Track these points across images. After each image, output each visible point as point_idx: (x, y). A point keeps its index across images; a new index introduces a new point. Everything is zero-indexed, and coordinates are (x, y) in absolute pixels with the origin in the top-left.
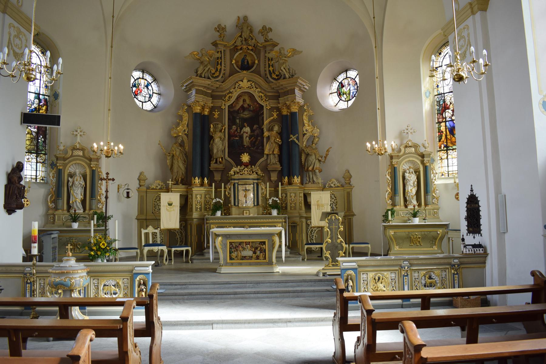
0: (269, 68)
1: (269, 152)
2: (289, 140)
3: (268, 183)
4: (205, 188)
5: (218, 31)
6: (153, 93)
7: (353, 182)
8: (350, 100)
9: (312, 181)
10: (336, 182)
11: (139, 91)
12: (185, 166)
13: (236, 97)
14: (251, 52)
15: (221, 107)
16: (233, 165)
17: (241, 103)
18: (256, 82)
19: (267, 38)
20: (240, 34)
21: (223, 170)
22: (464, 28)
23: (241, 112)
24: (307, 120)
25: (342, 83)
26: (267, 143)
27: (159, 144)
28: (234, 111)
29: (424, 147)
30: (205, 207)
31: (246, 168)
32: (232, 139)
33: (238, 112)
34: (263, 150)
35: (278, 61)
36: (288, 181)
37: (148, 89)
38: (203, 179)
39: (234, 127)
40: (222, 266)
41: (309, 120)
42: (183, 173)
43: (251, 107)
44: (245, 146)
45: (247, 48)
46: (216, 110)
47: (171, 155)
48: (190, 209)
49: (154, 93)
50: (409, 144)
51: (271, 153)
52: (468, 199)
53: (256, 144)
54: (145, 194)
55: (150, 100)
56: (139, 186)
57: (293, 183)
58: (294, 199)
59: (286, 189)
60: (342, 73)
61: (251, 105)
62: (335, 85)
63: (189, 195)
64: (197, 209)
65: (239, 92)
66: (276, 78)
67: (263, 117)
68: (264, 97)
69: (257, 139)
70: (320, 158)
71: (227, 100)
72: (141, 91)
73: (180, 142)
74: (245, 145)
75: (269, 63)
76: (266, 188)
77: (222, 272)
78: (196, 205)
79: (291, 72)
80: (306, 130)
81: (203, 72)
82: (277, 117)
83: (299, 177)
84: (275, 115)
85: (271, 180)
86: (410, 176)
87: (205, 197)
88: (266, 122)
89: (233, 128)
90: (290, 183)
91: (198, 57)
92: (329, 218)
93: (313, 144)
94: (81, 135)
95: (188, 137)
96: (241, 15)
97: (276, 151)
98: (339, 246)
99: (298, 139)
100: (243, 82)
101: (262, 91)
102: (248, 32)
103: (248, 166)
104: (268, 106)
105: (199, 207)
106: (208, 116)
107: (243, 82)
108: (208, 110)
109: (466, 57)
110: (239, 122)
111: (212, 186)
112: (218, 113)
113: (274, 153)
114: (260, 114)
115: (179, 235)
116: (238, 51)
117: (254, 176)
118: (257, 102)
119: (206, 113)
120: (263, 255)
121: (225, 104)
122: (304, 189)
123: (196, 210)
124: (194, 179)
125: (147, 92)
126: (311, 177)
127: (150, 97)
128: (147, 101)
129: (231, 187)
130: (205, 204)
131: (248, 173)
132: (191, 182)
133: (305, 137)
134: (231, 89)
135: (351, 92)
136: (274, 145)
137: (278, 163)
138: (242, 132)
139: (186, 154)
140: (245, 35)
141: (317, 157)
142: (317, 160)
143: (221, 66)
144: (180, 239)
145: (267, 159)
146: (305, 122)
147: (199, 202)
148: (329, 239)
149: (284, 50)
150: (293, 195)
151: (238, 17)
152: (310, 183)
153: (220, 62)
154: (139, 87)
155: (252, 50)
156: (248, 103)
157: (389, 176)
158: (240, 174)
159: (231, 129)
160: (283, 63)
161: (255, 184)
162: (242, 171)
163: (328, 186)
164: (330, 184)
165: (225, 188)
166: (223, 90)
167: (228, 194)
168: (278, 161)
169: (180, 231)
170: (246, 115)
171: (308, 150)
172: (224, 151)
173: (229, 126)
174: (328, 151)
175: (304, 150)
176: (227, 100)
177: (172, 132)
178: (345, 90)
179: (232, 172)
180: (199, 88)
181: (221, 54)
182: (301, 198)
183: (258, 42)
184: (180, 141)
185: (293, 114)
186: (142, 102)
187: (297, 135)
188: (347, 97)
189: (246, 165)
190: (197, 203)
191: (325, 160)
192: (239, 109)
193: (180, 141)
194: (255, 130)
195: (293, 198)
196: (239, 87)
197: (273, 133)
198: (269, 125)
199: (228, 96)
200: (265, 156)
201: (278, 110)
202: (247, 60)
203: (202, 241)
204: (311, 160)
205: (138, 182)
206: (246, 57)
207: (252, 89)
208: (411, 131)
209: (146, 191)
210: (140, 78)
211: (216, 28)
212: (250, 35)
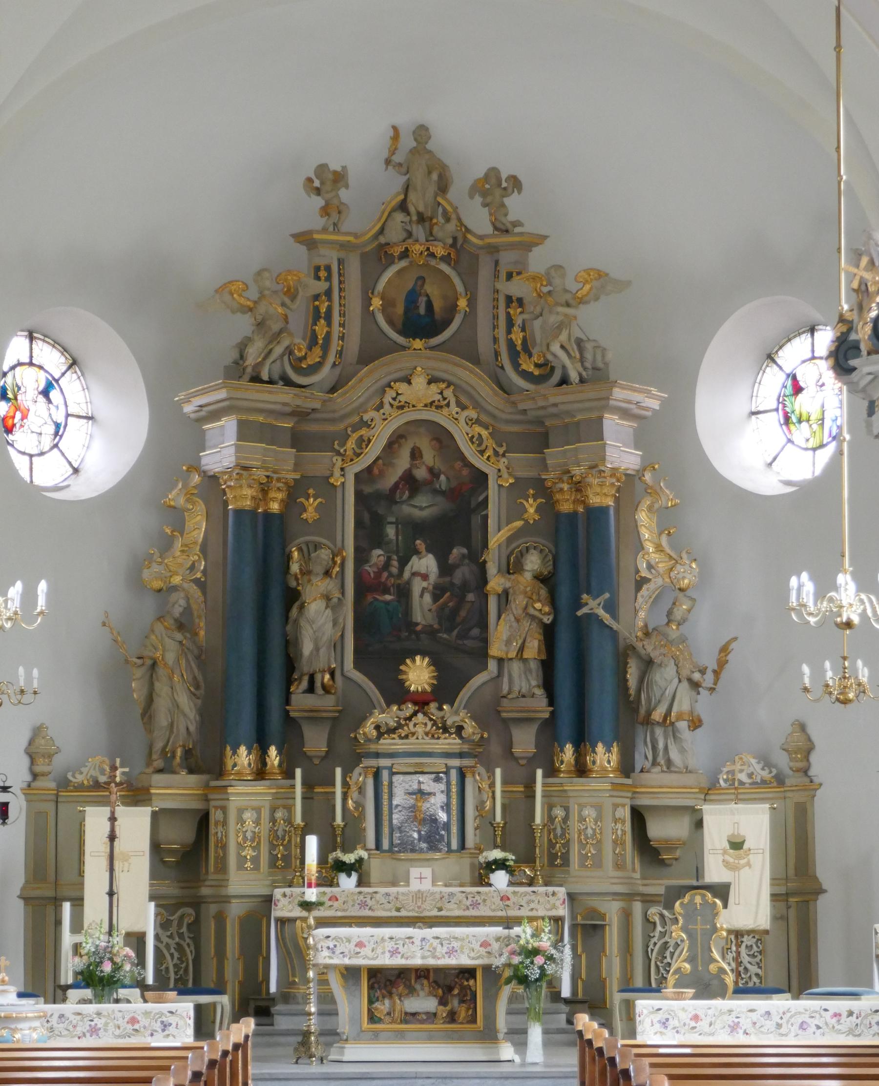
0: (509, 332)
1: (507, 654)
2: (579, 613)
3: (498, 772)
4: (270, 788)
5: (318, 192)
6: (68, 415)
7: (818, 766)
8: (822, 446)
9: (662, 762)
11: (18, 415)
12: (199, 702)
13: (384, 442)
14: (444, 267)
15: (328, 478)
16: (376, 703)
17: (403, 462)
18: (458, 382)
19: (503, 219)
20: (402, 197)
21: (334, 719)
23: (405, 497)
24: (654, 525)
26: (499, 617)
27: (104, 624)
28: (378, 496)
30: (239, 854)
31: (420, 716)
32: (370, 598)
33: (390, 498)
34: (485, 641)
35: (541, 315)
36: (577, 760)
37: (49, 401)
38: (264, 752)
39: (377, 555)
40: (347, 1040)
41: (662, 529)
42: (192, 728)
43: (443, 478)
44: (419, 628)
45: (428, 249)
46: (311, 491)
47: (149, 662)
48: (216, 863)
49: (73, 415)
51: (512, 654)
53: (459, 619)
54: (54, 808)
55: (56, 446)
56: (28, 778)
57: (591, 771)
58: (594, 830)
59: (565, 791)
60: (795, 337)
61: (443, 469)
63: (212, 811)
64: (242, 860)
65: (398, 421)
66: (537, 372)
67: (486, 518)
68: (491, 441)
69: (462, 599)
70: (697, 676)
71: (350, 453)
72: (25, 412)
73: (177, 615)
74: (417, 624)
75: (508, 314)
76: (492, 785)
77: (345, 1059)
78: (241, 847)
79: (589, 356)
80: (650, 567)
81: (265, 359)
82: (537, 517)
83: (615, 749)
84: (531, 510)
85: (512, 753)
87: (273, 820)
88: (496, 538)
89: (374, 560)
90: (581, 770)
91: (242, 301)
92: (686, 900)
93: (669, 622)
95: (204, 593)
96: (406, 120)
97: (534, 648)
98: (715, 982)
99: (611, 607)
100: (409, 383)
101: (484, 418)
102: (432, 189)
103: (427, 703)
104: (505, 475)
105: (249, 853)
106: (281, 516)
107: (409, 383)
108: (280, 496)
110: (397, 535)
111: (292, 776)
112: (319, 500)
113: (525, 656)
114: (473, 504)
115: (172, 955)
116: (393, 263)
117: (451, 743)
118: (463, 458)
119: (275, 507)
120: (468, 1009)
121: (342, 469)
122: (635, 793)
123: (241, 867)
124: (235, 753)
125: (45, 415)
126: (661, 745)
127: (56, 434)
128: (46, 448)
129: (364, 782)
130: (271, 843)
131: (427, 734)
132: (221, 763)
133: (644, 592)
134: (366, 412)
136: (526, 624)
137: (539, 692)
138: (407, 575)
139: (198, 658)
141: (685, 673)
142: (685, 684)
143: (329, 324)
144: (176, 973)
145: (500, 674)
146: (645, 534)
147: (249, 835)
148: (685, 961)
149: (563, 276)
150: (590, 813)
151: (395, 128)
152: (657, 769)
153: (323, 310)
154: (19, 397)
155: (446, 259)
156: (431, 464)
158: (401, 737)
159: (367, 561)
160: (560, 327)
161: (454, 774)
162: (407, 725)
163: (725, 781)
164: (732, 772)
165: (345, 784)
166: (336, 415)
167: (356, 808)
168: (538, 686)
169: (177, 944)
170: (421, 509)
171: (649, 648)
172: (338, 646)
173: (357, 549)
174: (725, 650)
175: (634, 648)
176: (350, 453)
177: (146, 574)
179: (368, 728)
180: (251, 418)
181: (329, 278)
182: (619, 826)
183: (468, 230)
184: (181, 609)
185: (597, 515)
187: (607, 595)
189: (421, 702)
190: (245, 839)
191: (715, 684)
192: (396, 486)
193: (177, 611)
194: (455, 567)
195: (590, 822)
196: (396, 404)
197: (521, 579)
198: (507, 546)
199: (355, 436)
200: (492, 665)
201: (543, 490)
202: (427, 295)
203: (261, 979)
204: (662, 683)
205: (25, 761)
206: (423, 285)
207: (445, 411)
209: (57, 796)
210: (20, 364)
211: (310, 180)
212: (440, 199)
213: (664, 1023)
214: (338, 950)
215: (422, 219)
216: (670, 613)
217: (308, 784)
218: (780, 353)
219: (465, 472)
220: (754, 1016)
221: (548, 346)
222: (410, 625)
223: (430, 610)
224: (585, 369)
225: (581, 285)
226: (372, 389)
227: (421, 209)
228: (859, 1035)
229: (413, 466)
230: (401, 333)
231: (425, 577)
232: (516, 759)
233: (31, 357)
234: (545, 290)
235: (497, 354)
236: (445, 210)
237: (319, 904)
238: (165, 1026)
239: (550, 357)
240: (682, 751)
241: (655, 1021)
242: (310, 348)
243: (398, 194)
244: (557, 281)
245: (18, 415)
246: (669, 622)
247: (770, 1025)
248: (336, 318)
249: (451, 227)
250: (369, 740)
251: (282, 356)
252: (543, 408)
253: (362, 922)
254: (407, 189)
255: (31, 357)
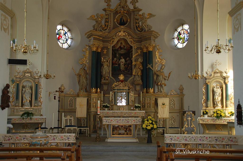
6: (68, 38)
7: (184, 92)
8: (184, 43)
10: (175, 92)
11: (60, 37)
14: (126, 15)
15: (108, 47)
17: (119, 45)
22: (239, 15)
25: (180, 32)
27: (72, 69)
28: (115, 50)
29: (206, 73)
31: (122, 83)
33: (117, 50)
37: (65, 36)
39: (115, 59)
43: (125, 47)
45: (124, 12)
46: (105, 49)
49: (69, 38)
50: (216, 71)
51: (136, 74)
52: (238, 106)
55: (66, 42)
62: (176, 34)
70: (165, 78)
74: (121, 70)
79: (149, 27)
86: (217, 90)
93: (161, 69)
94: (29, 64)
97: (140, 74)
99: (152, 67)
102: (124, 2)
103: (123, 82)
109: (238, 30)
115: (83, 121)
118: (129, 44)
119: (99, 51)
123: (93, 107)
134: (114, 37)
135: (185, 38)
136: (139, 69)
137: (140, 80)
138: (120, 62)
140: (122, 5)
141: (163, 77)
155: (126, 13)
157: (204, 89)
161: (127, 92)
163: (169, 94)
166: (109, 37)
171: (158, 73)
178: (182, 37)
179: (114, 86)
181: (108, 16)
186: (62, 44)
188: (183, 41)
189: (122, 81)
192: (118, 48)
199: (112, 41)
200: (133, 76)
201: (141, 49)
204: (160, 79)
206: (123, 18)
207: (126, 37)
208: (218, 64)
212: (126, 4)
213: (172, 139)
214: (107, 121)
215: (123, 7)
216: (161, 68)
217: (104, 95)
218: (177, 29)
219: (129, 46)
220: (190, 138)
221: (142, 25)
222: (120, 70)
223: (123, 68)
224: (148, 29)
225: (147, 16)
226: (115, 33)
227: (123, 5)
228: (212, 142)
229: (121, 45)
230: (119, 25)
231: (123, 62)
232: (137, 91)
233: (63, 29)
234: (142, 17)
235: (134, 28)
236: (126, 6)
237: (99, 114)
238: (68, 138)
239: (143, 27)
240: (163, 89)
241: (170, 139)
242: (105, 26)
243: (119, 3)
244: (144, 15)
245: (60, 37)
246: (161, 69)
247: (193, 140)
248: (109, 22)
249: (127, 8)
250: (113, 87)
251: (100, 27)
252: (141, 35)
253: (112, 117)
254: (120, 2)
255: (63, 29)
